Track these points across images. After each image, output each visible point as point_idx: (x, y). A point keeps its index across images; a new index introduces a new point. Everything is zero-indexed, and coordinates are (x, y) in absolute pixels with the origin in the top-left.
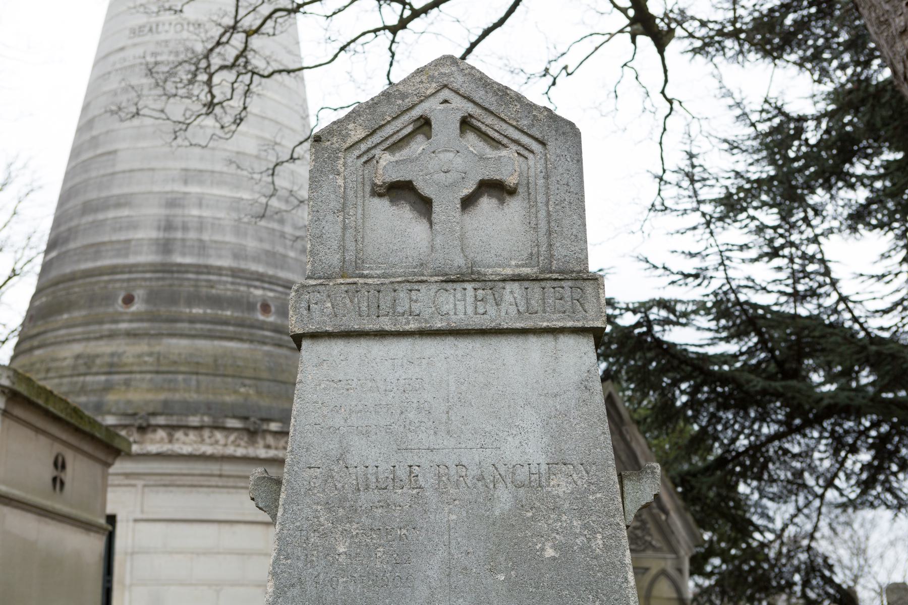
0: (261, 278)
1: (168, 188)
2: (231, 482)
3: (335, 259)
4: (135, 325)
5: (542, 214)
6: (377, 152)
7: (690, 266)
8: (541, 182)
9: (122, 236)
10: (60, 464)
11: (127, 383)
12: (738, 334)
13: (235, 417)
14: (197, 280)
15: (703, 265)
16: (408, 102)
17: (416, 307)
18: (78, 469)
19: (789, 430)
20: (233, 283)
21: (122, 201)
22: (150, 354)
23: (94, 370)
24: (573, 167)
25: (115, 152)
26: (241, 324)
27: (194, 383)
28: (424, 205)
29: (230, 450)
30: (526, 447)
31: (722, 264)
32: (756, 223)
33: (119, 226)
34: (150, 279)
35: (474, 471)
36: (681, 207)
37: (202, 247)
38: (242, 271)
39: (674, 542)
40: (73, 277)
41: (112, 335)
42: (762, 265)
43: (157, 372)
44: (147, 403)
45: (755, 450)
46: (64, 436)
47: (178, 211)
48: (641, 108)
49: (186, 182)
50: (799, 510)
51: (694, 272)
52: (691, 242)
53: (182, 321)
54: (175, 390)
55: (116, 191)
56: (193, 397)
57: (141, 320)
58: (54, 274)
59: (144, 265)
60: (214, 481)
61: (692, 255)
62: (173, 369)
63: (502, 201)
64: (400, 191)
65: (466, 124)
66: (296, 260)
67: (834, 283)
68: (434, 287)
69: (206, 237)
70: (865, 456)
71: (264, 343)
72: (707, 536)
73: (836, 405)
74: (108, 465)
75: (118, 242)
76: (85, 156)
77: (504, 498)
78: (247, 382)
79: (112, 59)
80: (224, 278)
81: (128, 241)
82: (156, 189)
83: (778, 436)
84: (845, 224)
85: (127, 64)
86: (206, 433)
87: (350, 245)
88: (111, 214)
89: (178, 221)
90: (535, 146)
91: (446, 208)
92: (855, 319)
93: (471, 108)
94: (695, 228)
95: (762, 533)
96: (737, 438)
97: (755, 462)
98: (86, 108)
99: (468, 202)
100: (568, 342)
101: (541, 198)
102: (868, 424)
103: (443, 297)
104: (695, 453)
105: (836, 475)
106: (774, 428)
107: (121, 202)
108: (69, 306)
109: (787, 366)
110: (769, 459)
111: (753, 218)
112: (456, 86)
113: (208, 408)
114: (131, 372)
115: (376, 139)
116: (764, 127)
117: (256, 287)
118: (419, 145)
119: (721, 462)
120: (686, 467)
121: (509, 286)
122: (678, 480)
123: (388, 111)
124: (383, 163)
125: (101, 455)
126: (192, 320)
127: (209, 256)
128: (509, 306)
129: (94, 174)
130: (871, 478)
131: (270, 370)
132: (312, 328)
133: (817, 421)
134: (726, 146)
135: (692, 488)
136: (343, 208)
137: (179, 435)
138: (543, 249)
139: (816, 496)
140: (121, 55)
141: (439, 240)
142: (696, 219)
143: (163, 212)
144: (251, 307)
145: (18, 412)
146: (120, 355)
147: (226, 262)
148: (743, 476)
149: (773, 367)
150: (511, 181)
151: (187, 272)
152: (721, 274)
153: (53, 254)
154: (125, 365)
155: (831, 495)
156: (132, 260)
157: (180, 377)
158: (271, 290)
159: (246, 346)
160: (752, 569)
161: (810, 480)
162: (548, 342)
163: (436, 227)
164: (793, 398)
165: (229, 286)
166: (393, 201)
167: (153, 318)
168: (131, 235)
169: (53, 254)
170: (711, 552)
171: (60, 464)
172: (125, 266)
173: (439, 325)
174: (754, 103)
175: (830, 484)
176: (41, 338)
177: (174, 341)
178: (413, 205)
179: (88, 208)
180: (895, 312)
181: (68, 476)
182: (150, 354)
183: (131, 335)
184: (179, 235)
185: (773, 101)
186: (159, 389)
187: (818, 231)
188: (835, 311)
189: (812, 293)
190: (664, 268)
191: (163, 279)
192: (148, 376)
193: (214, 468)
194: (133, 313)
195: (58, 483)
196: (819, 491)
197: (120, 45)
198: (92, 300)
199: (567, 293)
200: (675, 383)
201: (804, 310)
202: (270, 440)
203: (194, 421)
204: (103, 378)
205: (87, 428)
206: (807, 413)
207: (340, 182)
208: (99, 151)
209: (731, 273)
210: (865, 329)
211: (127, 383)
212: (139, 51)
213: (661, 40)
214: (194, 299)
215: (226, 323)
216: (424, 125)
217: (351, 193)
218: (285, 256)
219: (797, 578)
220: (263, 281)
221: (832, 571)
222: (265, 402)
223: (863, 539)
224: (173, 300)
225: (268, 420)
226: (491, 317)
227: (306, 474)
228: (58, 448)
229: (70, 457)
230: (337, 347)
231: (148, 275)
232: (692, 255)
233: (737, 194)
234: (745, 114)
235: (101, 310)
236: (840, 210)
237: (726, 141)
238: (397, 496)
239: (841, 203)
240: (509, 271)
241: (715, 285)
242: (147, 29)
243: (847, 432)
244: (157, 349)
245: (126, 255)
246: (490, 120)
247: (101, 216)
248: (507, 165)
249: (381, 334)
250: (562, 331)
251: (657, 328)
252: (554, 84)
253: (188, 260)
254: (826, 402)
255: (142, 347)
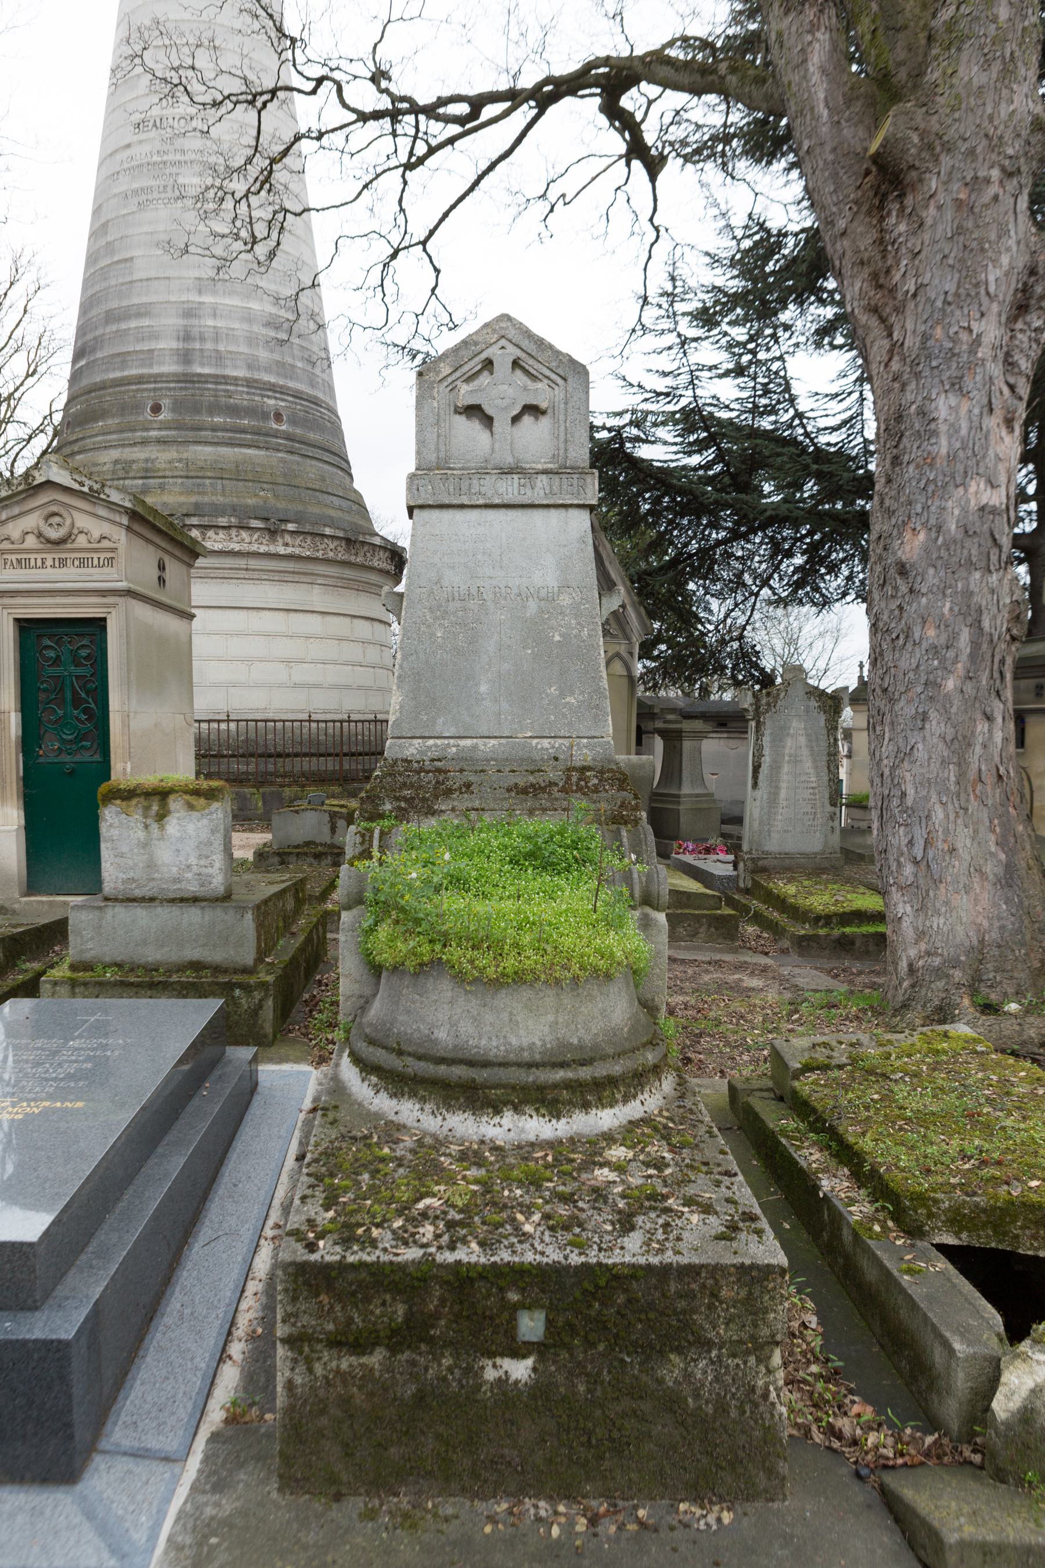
0: (273, 388)
1: (184, 298)
2: (256, 575)
3: (433, 457)
4: (163, 433)
5: (562, 428)
6: (458, 383)
7: (661, 384)
8: (562, 406)
9: (145, 346)
10: (162, 567)
11: (162, 487)
12: (700, 446)
13: (256, 518)
14: (216, 390)
15: (674, 384)
16: (479, 348)
17: (483, 490)
18: (173, 569)
19: (736, 535)
20: (248, 393)
21: (143, 310)
22: (180, 461)
23: (131, 474)
24: (583, 396)
25: (132, 259)
26: (257, 432)
27: (219, 487)
28: (488, 421)
29: (254, 548)
30: (546, 577)
31: (692, 382)
32: (728, 338)
33: (143, 335)
34: (175, 389)
35: (515, 591)
36: (659, 327)
37: (219, 358)
38: (256, 381)
39: (628, 631)
40: (103, 386)
41: (144, 442)
42: (728, 381)
43: (187, 477)
44: (181, 505)
45: (705, 553)
46: (163, 544)
47: (195, 322)
48: (632, 322)
49: (200, 292)
50: (736, 605)
51: (665, 390)
52: (665, 362)
53: (206, 429)
54: (204, 493)
55: (136, 301)
56: (220, 499)
57: (170, 429)
58: (85, 382)
59: (168, 375)
60: (242, 574)
61: (665, 374)
62: (200, 474)
63: (537, 418)
64: (473, 411)
65: (516, 364)
66: (303, 369)
67: (792, 400)
68: (494, 477)
69: (221, 348)
70: (799, 560)
71: (278, 450)
72: (657, 625)
73: (777, 516)
74: (190, 566)
75: (142, 351)
76: (102, 263)
77: (533, 606)
78: (265, 486)
79: (119, 157)
80: (240, 388)
81: (151, 351)
82: (173, 299)
83: (724, 542)
84: (811, 340)
85: (134, 163)
86: (234, 532)
87: (442, 448)
88: (133, 324)
89: (195, 332)
90: (560, 381)
91: (501, 423)
92: (807, 434)
93: (519, 353)
94: (670, 348)
95: (703, 624)
96: (689, 543)
97: (704, 565)
98: (97, 211)
99: (515, 419)
100: (574, 513)
101: (562, 417)
102: (804, 532)
103: (500, 483)
104: (654, 553)
105: (770, 577)
106: (722, 534)
107: (142, 311)
108: (103, 414)
109: (740, 479)
110: (714, 562)
111: (726, 334)
112: (510, 336)
113: (234, 510)
114: (164, 477)
115: (458, 374)
116: (747, 244)
117: (269, 397)
118: (485, 379)
119: (675, 562)
120: (643, 565)
121: (540, 477)
122: (635, 578)
123: (466, 354)
124: (462, 392)
125: (186, 558)
126: (214, 429)
127: (225, 366)
128: (540, 489)
129: (113, 282)
130: (806, 578)
131: (285, 475)
132: (420, 502)
133: (763, 528)
134: (708, 260)
135: (648, 585)
136: (438, 423)
137: (211, 533)
138: (562, 452)
139: (752, 594)
140: (128, 153)
141: (497, 445)
142: (672, 339)
143: (181, 322)
144: (265, 416)
145: (136, 527)
146: (153, 461)
147: (241, 373)
148: (692, 576)
149: (727, 480)
150: (544, 405)
151: (207, 382)
152: (690, 393)
153: (82, 363)
154: (159, 470)
155: (766, 592)
156: (156, 370)
157: (208, 481)
158: (283, 400)
159: (263, 453)
160: (692, 654)
161: (747, 578)
162: (562, 512)
163: (496, 437)
164: (741, 509)
165: (245, 396)
166: (468, 417)
167: (179, 426)
168: (123, 326)
169: (82, 363)
170: (658, 640)
171: (162, 567)
172: (150, 376)
173: (497, 501)
174: (739, 220)
175: (765, 583)
176: (81, 443)
177: (199, 448)
178: (481, 420)
179: (111, 317)
180: (844, 430)
181: (168, 575)
182: (180, 461)
183: (160, 441)
184: (197, 345)
185: (755, 217)
186: (191, 492)
187: (784, 349)
188: (790, 426)
189: (772, 410)
190: (639, 386)
191: (186, 389)
192: (180, 481)
193: (242, 562)
194: (161, 422)
195: (161, 580)
196: (755, 589)
197: (127, 142)
198: (124, 409)
199: (575, 482)
200: (640, 494)
201: (766, 423)
202: (288, 538)
203: (223, 521)
204: (140, 482)
205: (179, 538)
206: (752, 520)
207: (435, 404)
208: (116, 259)
209: (699, 392)
210: (815, 445)
211: (162, 487)
212: (147, 148)
213: (654, 167)
214: (214, 408)
215: (244, 431)
216: (488, 364)
217: (442, 412)
218: (293, 366)
219: (728, 662)
220: (275, 391)
221: (758, 658)
222: (282, 505)
223: (796, 630)
224: (196, 409)
225: (287, 521)
226: (529, 497)
227: (418, 591)
228: (160, 554)
229: (167, 559)
230: (435, 514)
231: (172, 385)
232: (665, 374)
233: (714, 306)
234: (728, 226)
235: (133, 418)
236: (809, 325)
237: (707, 254)
238: (471, 604)
239: (810, 318)
240: (540, 467)
241: (684, 402)
242: (151, 124)
243: (784, 539)
244: (185, 455)
245: (151, 365)
246: (531, 362)
247: (123, 326)
248: (541, 394)
249: (462, 506)
250: (571, 506)
251: (628, 445)
252: (552, 210)
253: (207, 371)
254: (768, 513)
255: (172, 453)
